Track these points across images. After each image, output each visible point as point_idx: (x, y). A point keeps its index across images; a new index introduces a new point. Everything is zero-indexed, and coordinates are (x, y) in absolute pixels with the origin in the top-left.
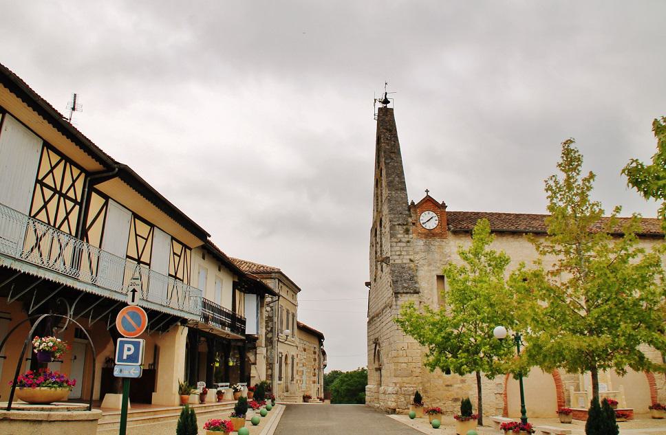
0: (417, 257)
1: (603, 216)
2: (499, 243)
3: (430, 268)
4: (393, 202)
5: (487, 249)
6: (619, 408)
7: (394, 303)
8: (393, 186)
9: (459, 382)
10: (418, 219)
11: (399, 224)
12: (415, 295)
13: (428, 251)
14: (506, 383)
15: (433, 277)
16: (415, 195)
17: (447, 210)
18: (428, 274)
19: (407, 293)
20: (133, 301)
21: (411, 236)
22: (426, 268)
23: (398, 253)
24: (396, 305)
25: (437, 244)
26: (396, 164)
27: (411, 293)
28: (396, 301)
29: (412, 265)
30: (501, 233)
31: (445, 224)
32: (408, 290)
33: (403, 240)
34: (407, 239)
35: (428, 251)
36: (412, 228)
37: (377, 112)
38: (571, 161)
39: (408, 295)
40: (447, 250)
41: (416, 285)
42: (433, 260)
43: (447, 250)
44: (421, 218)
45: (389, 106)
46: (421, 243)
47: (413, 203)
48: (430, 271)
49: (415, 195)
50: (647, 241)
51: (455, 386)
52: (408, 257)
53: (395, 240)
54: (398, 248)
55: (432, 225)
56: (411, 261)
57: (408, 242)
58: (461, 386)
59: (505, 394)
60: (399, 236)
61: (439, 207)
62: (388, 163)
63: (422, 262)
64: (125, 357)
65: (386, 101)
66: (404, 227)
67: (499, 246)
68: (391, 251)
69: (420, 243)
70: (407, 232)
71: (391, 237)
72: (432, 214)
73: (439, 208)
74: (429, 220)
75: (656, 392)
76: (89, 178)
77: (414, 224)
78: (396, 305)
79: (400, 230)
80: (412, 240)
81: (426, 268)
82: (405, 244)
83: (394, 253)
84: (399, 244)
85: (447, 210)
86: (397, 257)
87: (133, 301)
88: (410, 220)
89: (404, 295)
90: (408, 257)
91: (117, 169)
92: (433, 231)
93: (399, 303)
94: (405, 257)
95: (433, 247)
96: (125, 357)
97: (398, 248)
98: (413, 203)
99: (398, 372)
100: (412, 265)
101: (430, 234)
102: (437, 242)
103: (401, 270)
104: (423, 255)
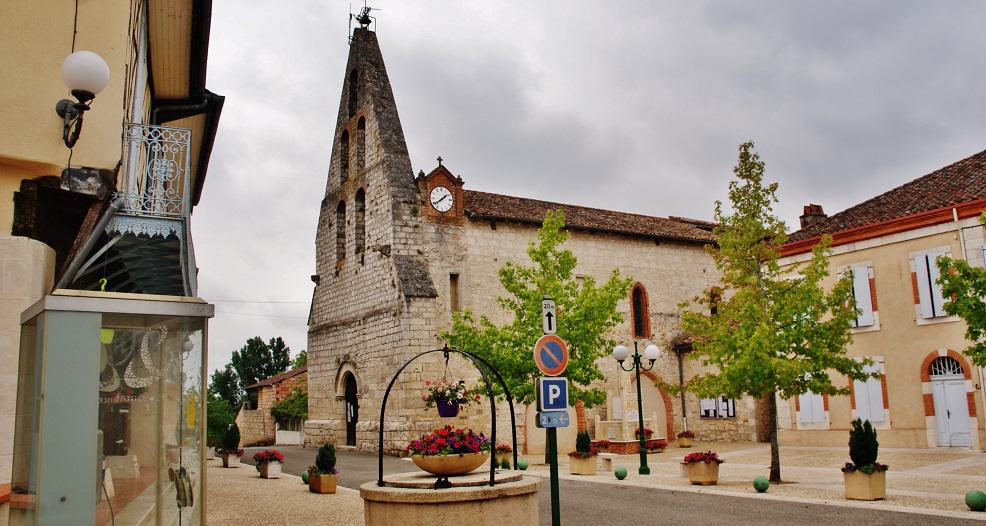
0: (427, 248)
1: (787, 233)
2: (521, 238)
3: (443, 264)
4: (394, 170)
5: (560, 248)
6: (653, 437)
7: (406, 310)
8: (391, 147)
9: (475, 412)
10: (428, 197)
11: (405, 202)
12: (431, 300)
13: (441, 241)
14: (526, 413)
15: (446, 275)
16: (422, 162)
17: (464, 187)
18: (440, 271)
19: (421, 297)
20: (550, 329)
21: (419, 219)
22: (437, 263)
23: (403, 241)
24: (408, 313)
25: (451, 232)
26: (390, 116)
27: (426, 297)
28: (408, 307)
29: (420, 258)
30: (578, 231)
31: (460, 206)
32: (423, 293)
33: (410, 223)
34: (415, 223)
35: (441, 241)
36: (421, 209)
37: (352, 34)
38: (749, 166)
39: (423, 299)
40: (463, 241)
41: (431, 287)
42: (446, 253)
43: (463, 241)
44: (451, 203)
45: (371, 28)
46: (432, 229)
47: (422, 174)
48: (442, 268)
49: (422, 162)
50: (672, 246)
51: (471, 418)
52: (416, 248)
53: (400, 223)
54: (403, 235)
55: (445, 206)
56: (419, 252)
57: (416, 227)
58: (477, 417)
59: (525, 427)
60: (405, 217)
61: (454, 183)
62: (381, 113)
63: (433, 255)
64: (551, 402)
65: (365, 20)
66: (412, 206)
67: (571, 245)
68: (394, 238)
69: (431, 230)
70: (414, 213)
71: (394, 219)
72: (445, 191)
73: (454, 184)
74: (442, 199)
75: (672, 419)
76: (157, 110)
77: (423, 202)
78: (408, 313)
79: (406, 209)
80: (421, 225)
81: (437, 263)
82: (411, 230)
83: (398, 241)
84: (405, 229)
85: (464, 187)
86: (401, 247)
87: (550, 329)
88: (419, 197)
89: (418, 299)
90: (416, 248)
91: (206, 101)
92: (445, 215)
93: (412, 309)
94: (412, 247)
95: (446, 237)
96: (551, 402)
97: (403, 235)
98: (422, 174)
99: (411, 402)
100: (420, 258)
101: (442, 219)
102: (451, 230)
103: (409, 265)
104: (434, 245)
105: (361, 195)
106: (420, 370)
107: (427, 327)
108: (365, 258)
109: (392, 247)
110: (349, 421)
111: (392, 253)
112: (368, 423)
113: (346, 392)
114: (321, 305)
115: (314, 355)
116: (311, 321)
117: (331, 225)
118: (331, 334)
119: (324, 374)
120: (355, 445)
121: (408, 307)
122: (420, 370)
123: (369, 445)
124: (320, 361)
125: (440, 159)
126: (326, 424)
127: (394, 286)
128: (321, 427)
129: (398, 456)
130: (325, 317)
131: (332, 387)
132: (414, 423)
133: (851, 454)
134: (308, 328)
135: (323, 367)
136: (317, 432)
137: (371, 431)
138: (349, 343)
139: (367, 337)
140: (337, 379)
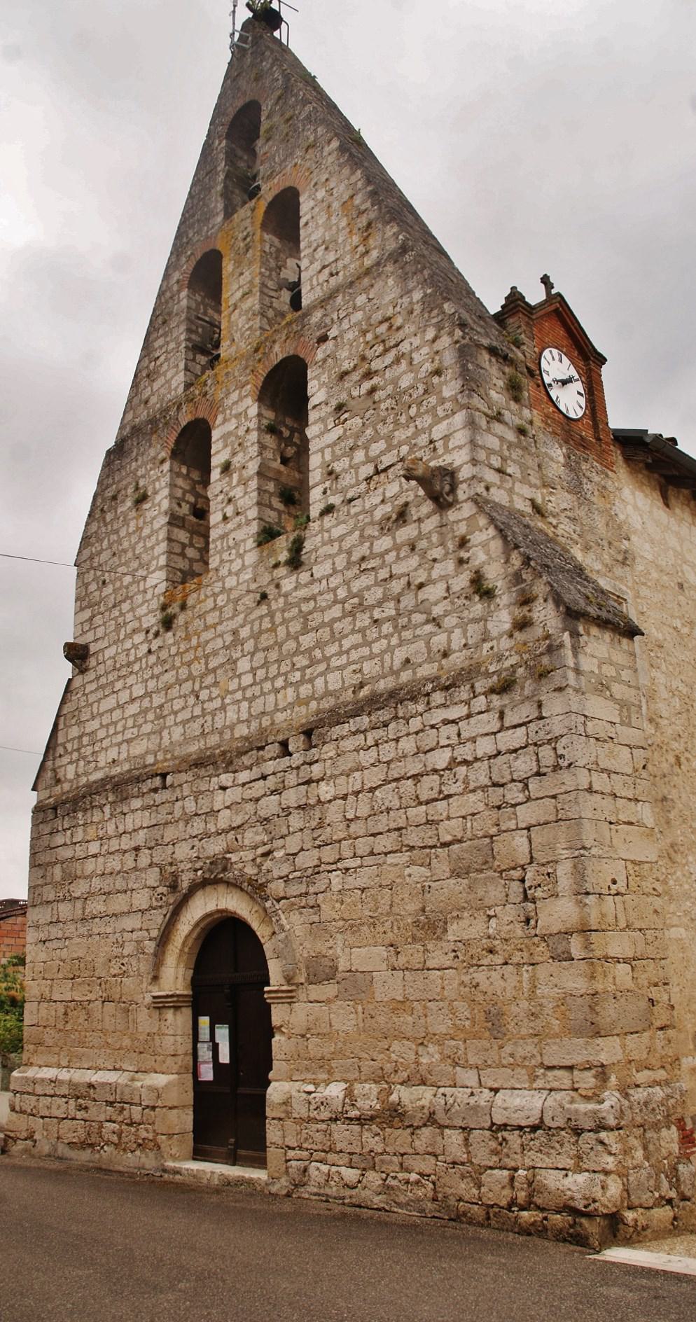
24: (577, 671)
28: (576, 650)
52: (527, 492)
56: (538, 510)
78: (577, 671)
105: (285, 390)
106: (621, 886)
107: (627, 734)
108: (308, 546)
109: (465, 473)
110: (207, 1073)
111: (462, 492)
112: (335, 1091)
113: (195, 983)
114: (95, 724)
115: (57, 871)
116: (46, 774)
117: (142, 499)
118: (136, 803)
119: (98, 927)
120: (261, 1163)
121: (576, 650)
122: (621, 886)
123: (351, 1175)
124: (80, 888)
125: (545, 280)
126: (113, 1088)
127: (487, 594)
128: (82, 1094)
129: (580, 1240)
130: (103, 760)
131: (145, 966)
132: (627, 1096)
133: (269, 1031)
134: (32, 799)
135: (96, 906)
136: (59, 1107)
137: (360, 1121)
138: (225, 819)
139: (326, 791)
140: (163, 940)
